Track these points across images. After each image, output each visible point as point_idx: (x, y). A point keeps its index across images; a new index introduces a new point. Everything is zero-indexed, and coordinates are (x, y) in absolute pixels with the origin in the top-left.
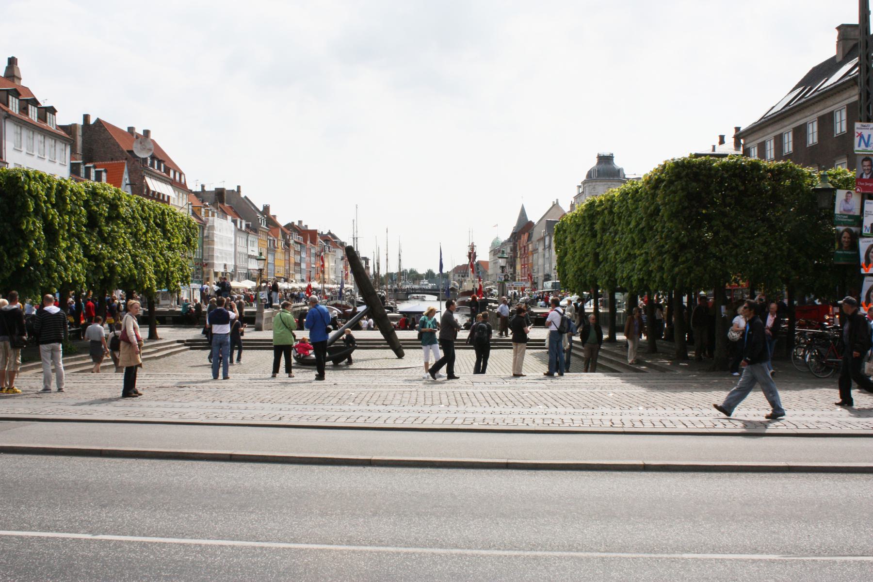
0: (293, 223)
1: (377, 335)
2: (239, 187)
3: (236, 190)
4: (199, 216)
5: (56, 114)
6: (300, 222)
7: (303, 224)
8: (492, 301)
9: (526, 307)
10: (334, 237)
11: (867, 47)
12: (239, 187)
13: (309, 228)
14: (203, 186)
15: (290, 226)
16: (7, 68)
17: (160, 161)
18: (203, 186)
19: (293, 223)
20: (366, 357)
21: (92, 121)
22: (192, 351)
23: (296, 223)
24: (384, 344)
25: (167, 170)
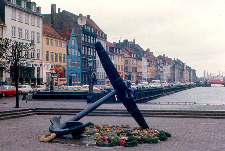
0: (161, 55)
1: (121, 107)
2: (134, 40)
3: (133, 41)
4: (113, 51)
6: (164, 55)
7: (166, 56)
8: (3, 66)
9: (160, 64)
10: (180, 61)
11: (168, 123)
12: (134, 40)
13: (168, 57)
14: (119, 41)
15: (160, 57)
16: (203, 86)
17: (91, 27)
18: (119, 41)
19: (161, 55)
20: (215, 86)
21: (61, 11)
22: (37, 116)
23: (163, 56)
24: (126, 113)
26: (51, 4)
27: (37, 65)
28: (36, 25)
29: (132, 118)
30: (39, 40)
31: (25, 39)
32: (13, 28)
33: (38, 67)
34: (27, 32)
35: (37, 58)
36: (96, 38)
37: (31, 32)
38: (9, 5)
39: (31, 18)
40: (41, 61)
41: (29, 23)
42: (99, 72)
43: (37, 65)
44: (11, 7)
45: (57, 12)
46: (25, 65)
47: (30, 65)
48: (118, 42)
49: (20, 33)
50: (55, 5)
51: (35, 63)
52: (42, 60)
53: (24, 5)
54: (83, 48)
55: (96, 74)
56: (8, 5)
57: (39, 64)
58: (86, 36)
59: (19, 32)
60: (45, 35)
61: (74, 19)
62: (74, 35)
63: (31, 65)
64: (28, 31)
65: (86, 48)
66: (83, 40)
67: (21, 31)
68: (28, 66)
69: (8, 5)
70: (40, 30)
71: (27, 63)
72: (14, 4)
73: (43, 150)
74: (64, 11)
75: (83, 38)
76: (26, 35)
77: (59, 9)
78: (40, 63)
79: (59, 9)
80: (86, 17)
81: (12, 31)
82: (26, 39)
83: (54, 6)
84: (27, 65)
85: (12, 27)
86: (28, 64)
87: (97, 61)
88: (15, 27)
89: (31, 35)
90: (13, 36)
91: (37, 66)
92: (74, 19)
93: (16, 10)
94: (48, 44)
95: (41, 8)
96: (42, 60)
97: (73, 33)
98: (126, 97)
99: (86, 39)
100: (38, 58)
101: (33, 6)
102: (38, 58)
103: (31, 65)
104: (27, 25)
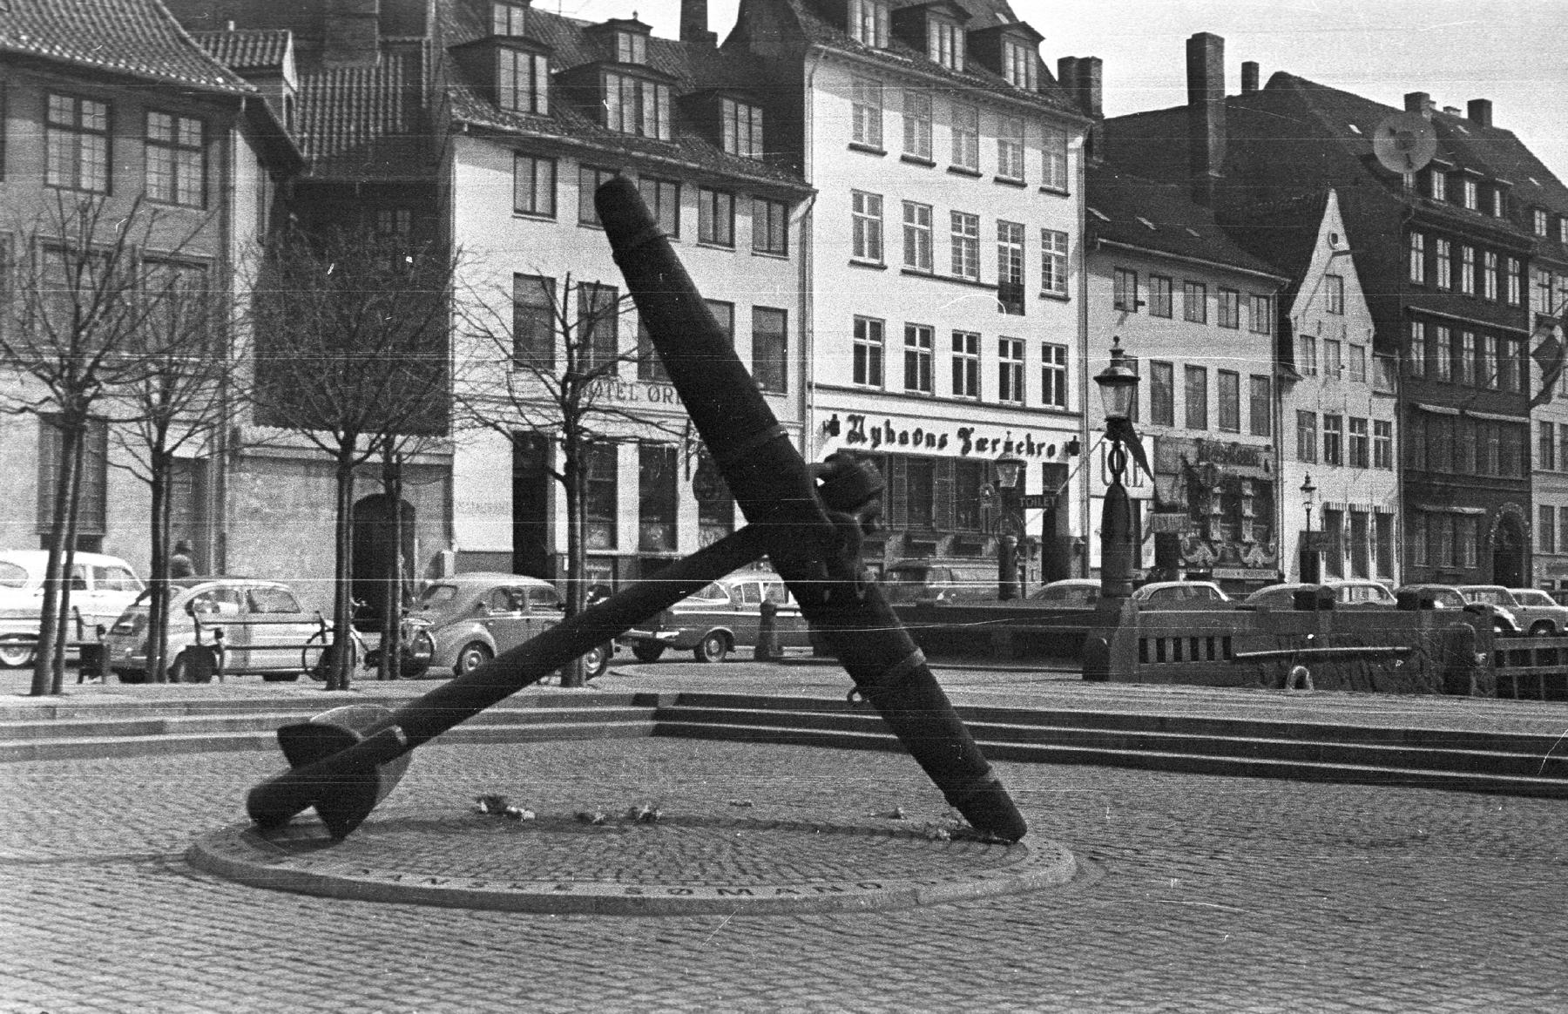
5: (1042, 45)
25: (1520, 211)
26: (1190, 37)
27: (1041, 446)
28: (1034, 176)
29: (911, 762)
30: (1060, 279)
31: (949, 274)
32: (866, 203)
33: (1047, 460)
34: (973, 232)
35: (1046, 400)
36: (1525, 261)
37: (1002, 226)
38: (827, 52)
39: (1001, 132)
40: (1074, 424)
41: (934, 160)
42: (1372, 474)
43: (1044, 450)
44: (847, 62)
45: (1233, 87)
46: (953, 449)
47: (989, 445)
48: (631, 17)
49: (866, 225)
50: (1218, 42)
51: (1028, 436)
52: (1079, 416)
53: (948, 49)
54: (1418, 330)
55: (1529, 518)
56: (823, 54)
57: (1060, 441)
58: (1442, 247)
59: (909, 232)
60: (1102, 244)
61: (1353, 127)
62: (1343, 244)
63: (994, 450)
64: (974, 219)
65: (1442, 334)
66: (1417, 274)
67: (924, 221)
68: (973, 454)
69: (823, 54)
70: (1067, 215)
71: (964, 434)
72: (953, 63)
73: (1296, 1009)
74: (1279, 78)
75: (1417, 261)
76: (957, 251)
77: (1249, 70)
78: (1069, 437)
79: (1249, 70)
80: (1464, 115)
81: (858, 222)
82: (956, 275)
83: (1209, 47)
84: (966, 448)
85: (858, 197)
86: (974, 438)
87: (1535, 427)
88: (876, 201)
89: (1002, 250)
90: (866, 259)
91: (1044, 458)
92: (1353, 127)
93: (1023, 120)
94: (1232, 321)
95: (1105, 67)
96: (1079, 416)
97: (1335, 231)
98: (664, 530)
99: (1490, 279)
100: (1012, 394)
101: (1021, 51)
102: (1012, 394)
103: (994, 450)
104: (968, 181)
